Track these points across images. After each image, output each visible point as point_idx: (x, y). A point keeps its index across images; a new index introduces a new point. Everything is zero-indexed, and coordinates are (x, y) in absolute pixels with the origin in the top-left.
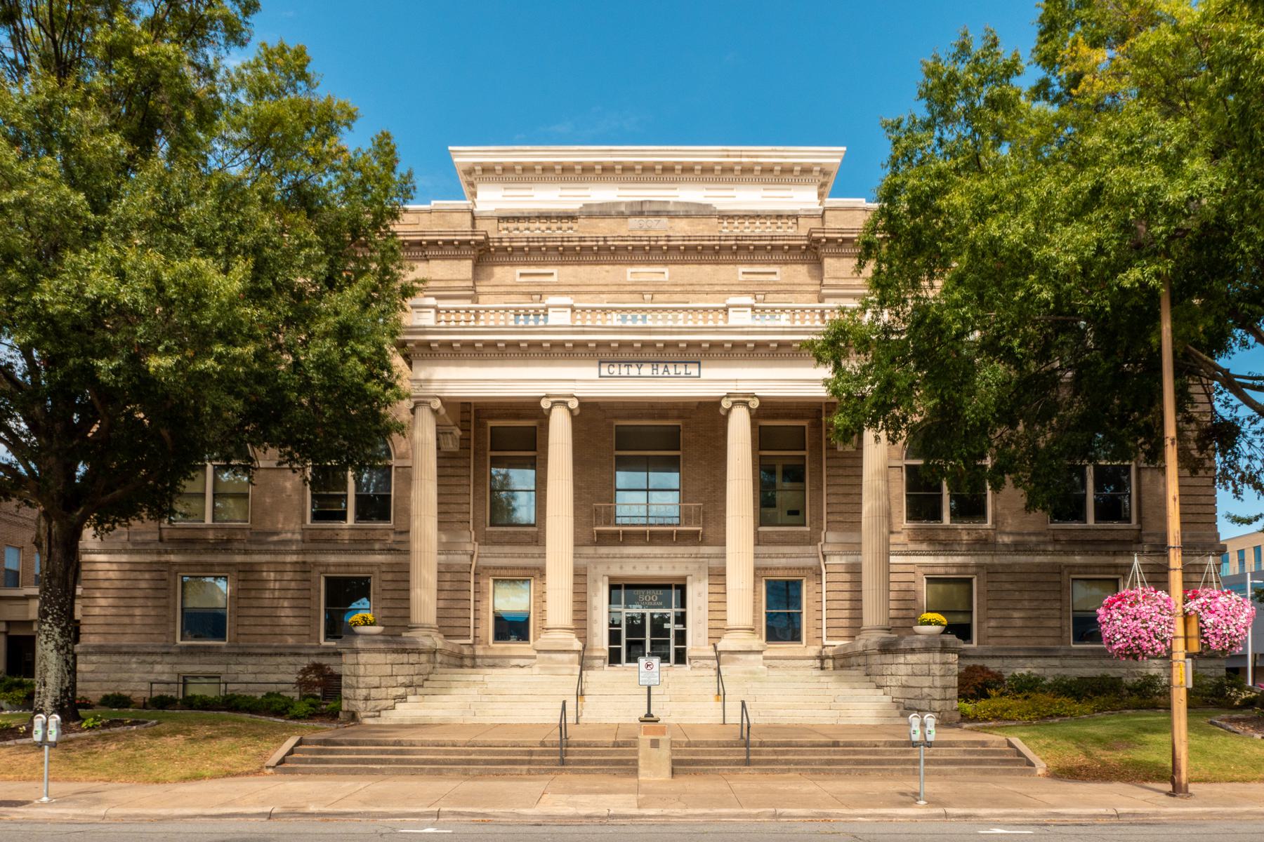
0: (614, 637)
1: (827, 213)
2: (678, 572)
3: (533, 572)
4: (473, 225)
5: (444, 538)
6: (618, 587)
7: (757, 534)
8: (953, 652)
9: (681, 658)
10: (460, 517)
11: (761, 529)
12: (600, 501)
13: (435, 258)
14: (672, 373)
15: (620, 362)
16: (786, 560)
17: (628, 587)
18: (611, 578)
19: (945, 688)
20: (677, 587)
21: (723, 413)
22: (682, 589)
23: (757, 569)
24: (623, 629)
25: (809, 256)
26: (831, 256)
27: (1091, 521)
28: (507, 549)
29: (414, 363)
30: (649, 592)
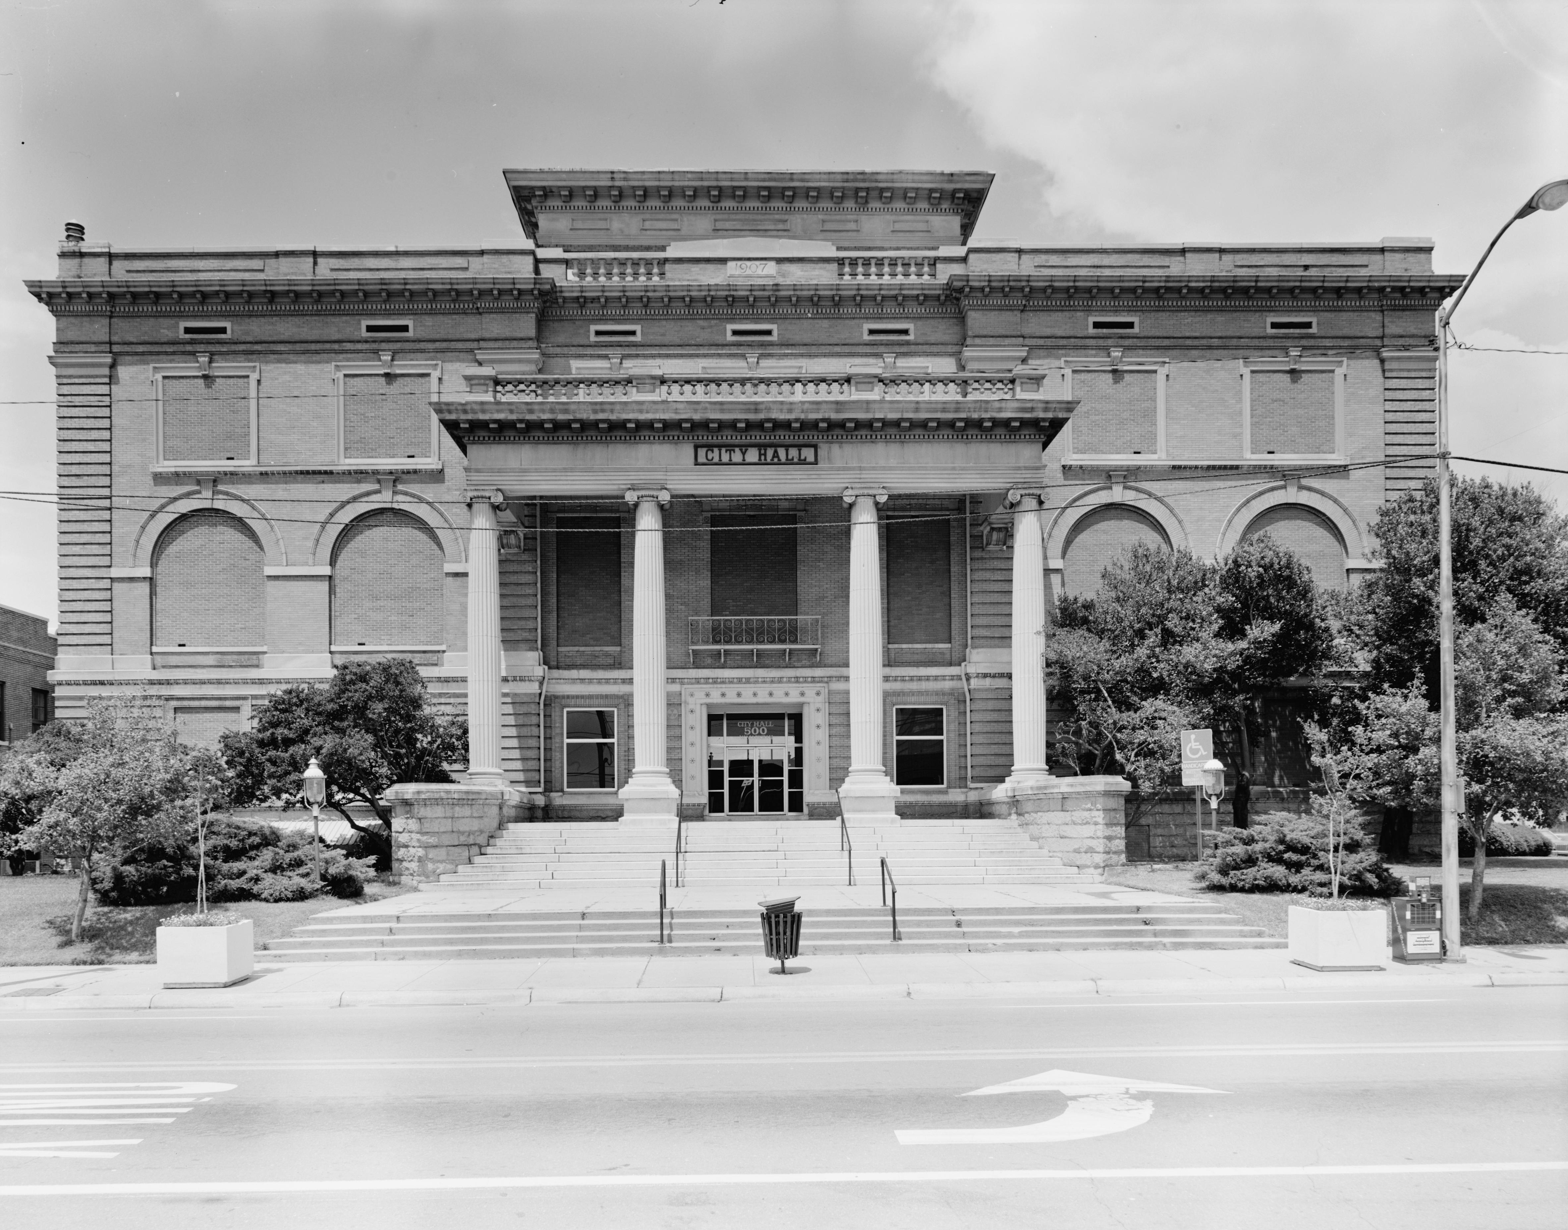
0: (715, 779)
1: (972, 256)
2: (794, 698)
3: (616, 702)
4: (537, 271)
5: (1436, 850)
6: (719, 717)
7: (887, 652)
8: (153, 573)
9: (796, 805)
10: (526, 635)
11: (890, 646)
12: (697, 614)
13: (490, 311)
14: (783, 457)
15: (720, 447)
16: (928, 684)
17: (731, 717)
18: (709, 706)
19: (1109, 838)
20: (791, 716)
21: (845, 506)
22: (797, 720)
23: (886, 695)
24: (726, 769)
25: (951, 309)
26: (974, 308)
27: (567, 741)
28: (584, 674)
29: (469, 447)
30: (756, 723)
